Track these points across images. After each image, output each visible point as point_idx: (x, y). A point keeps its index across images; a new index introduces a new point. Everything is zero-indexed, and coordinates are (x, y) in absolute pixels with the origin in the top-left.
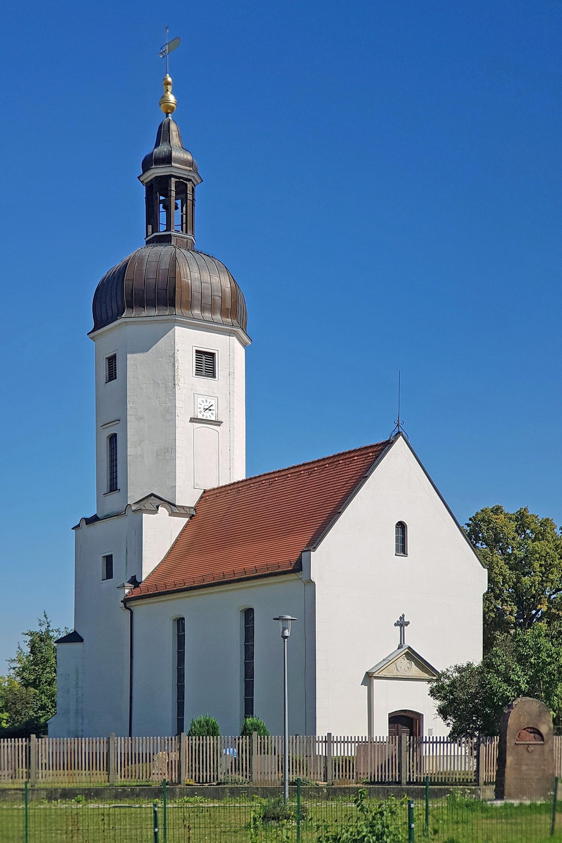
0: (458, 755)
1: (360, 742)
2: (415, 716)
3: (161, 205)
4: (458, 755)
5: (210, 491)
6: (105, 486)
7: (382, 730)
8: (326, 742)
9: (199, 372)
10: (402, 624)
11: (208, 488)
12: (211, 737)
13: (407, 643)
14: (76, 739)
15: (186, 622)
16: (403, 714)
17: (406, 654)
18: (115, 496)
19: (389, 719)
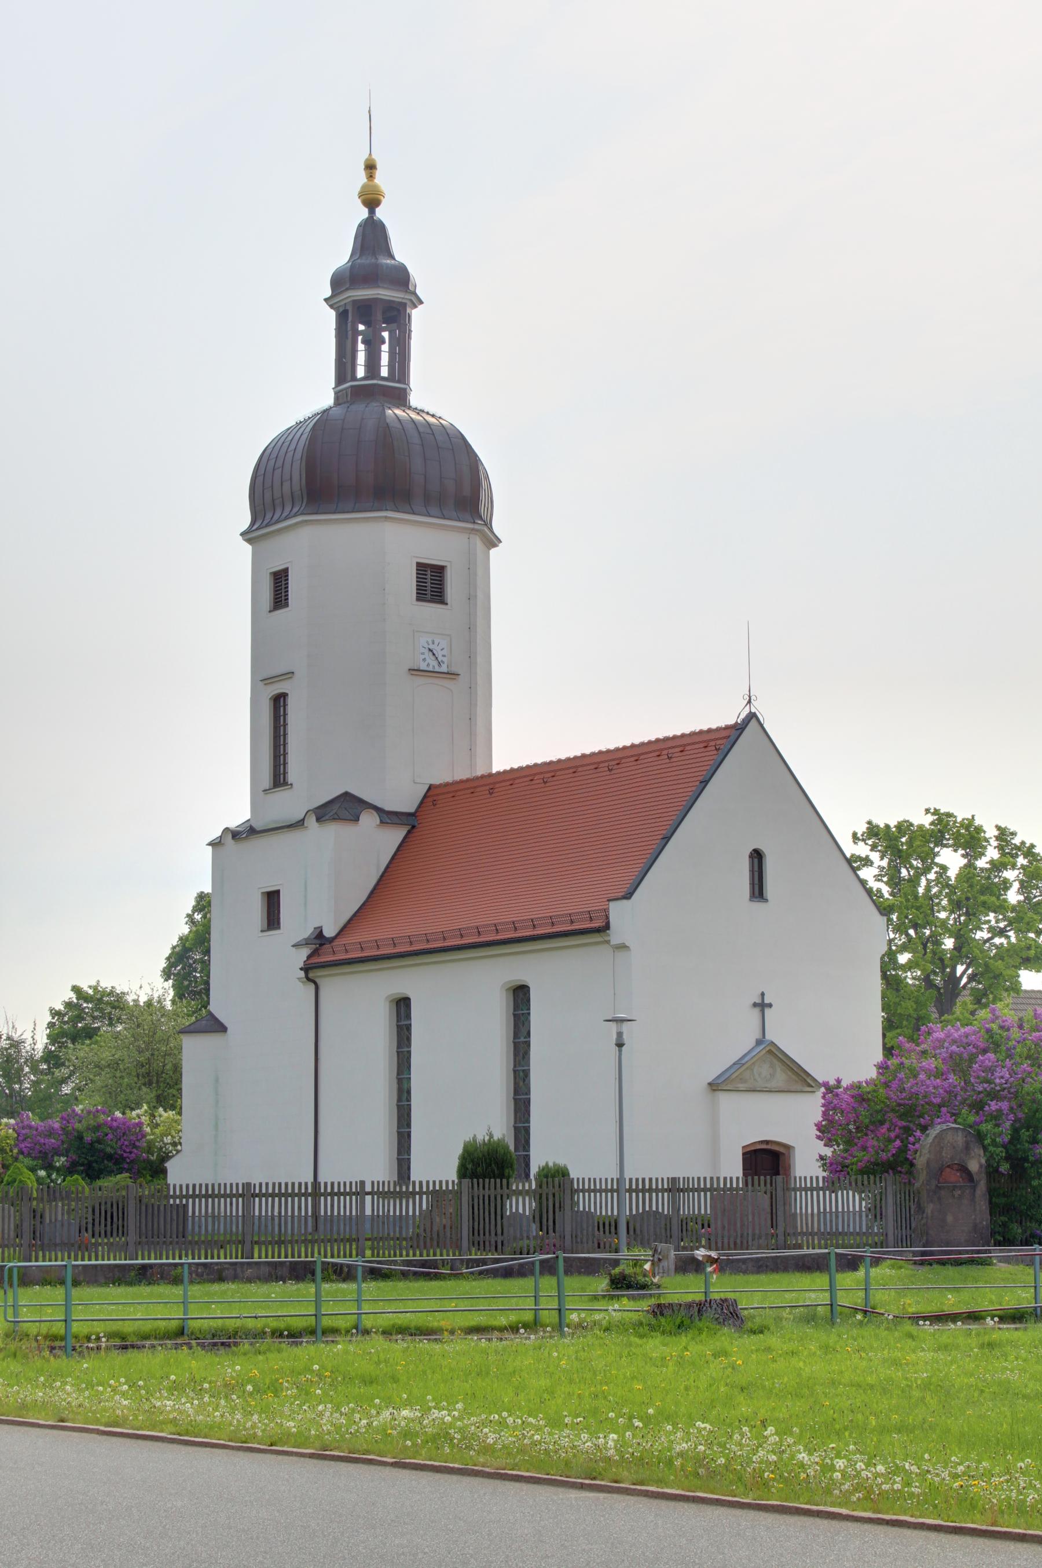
0: (831, 1212)
1: (715, 1190)
2: (782, 1150)
3: (360, 338)
4: (831, 1212)
5: (440, 785)
6: (266, 780)
7: (733, 1169)
8: (669, 1190)
9: (422, 595)
10: (762, 1006)
11: (437, 782)
12: (872, 1177)
13: (768, 1037)
14: (756, 1178)
15: (291, 701)
16: (759, 1147)
17: (770, 1052)
18: (281, 795)
19: (744, 1154)
